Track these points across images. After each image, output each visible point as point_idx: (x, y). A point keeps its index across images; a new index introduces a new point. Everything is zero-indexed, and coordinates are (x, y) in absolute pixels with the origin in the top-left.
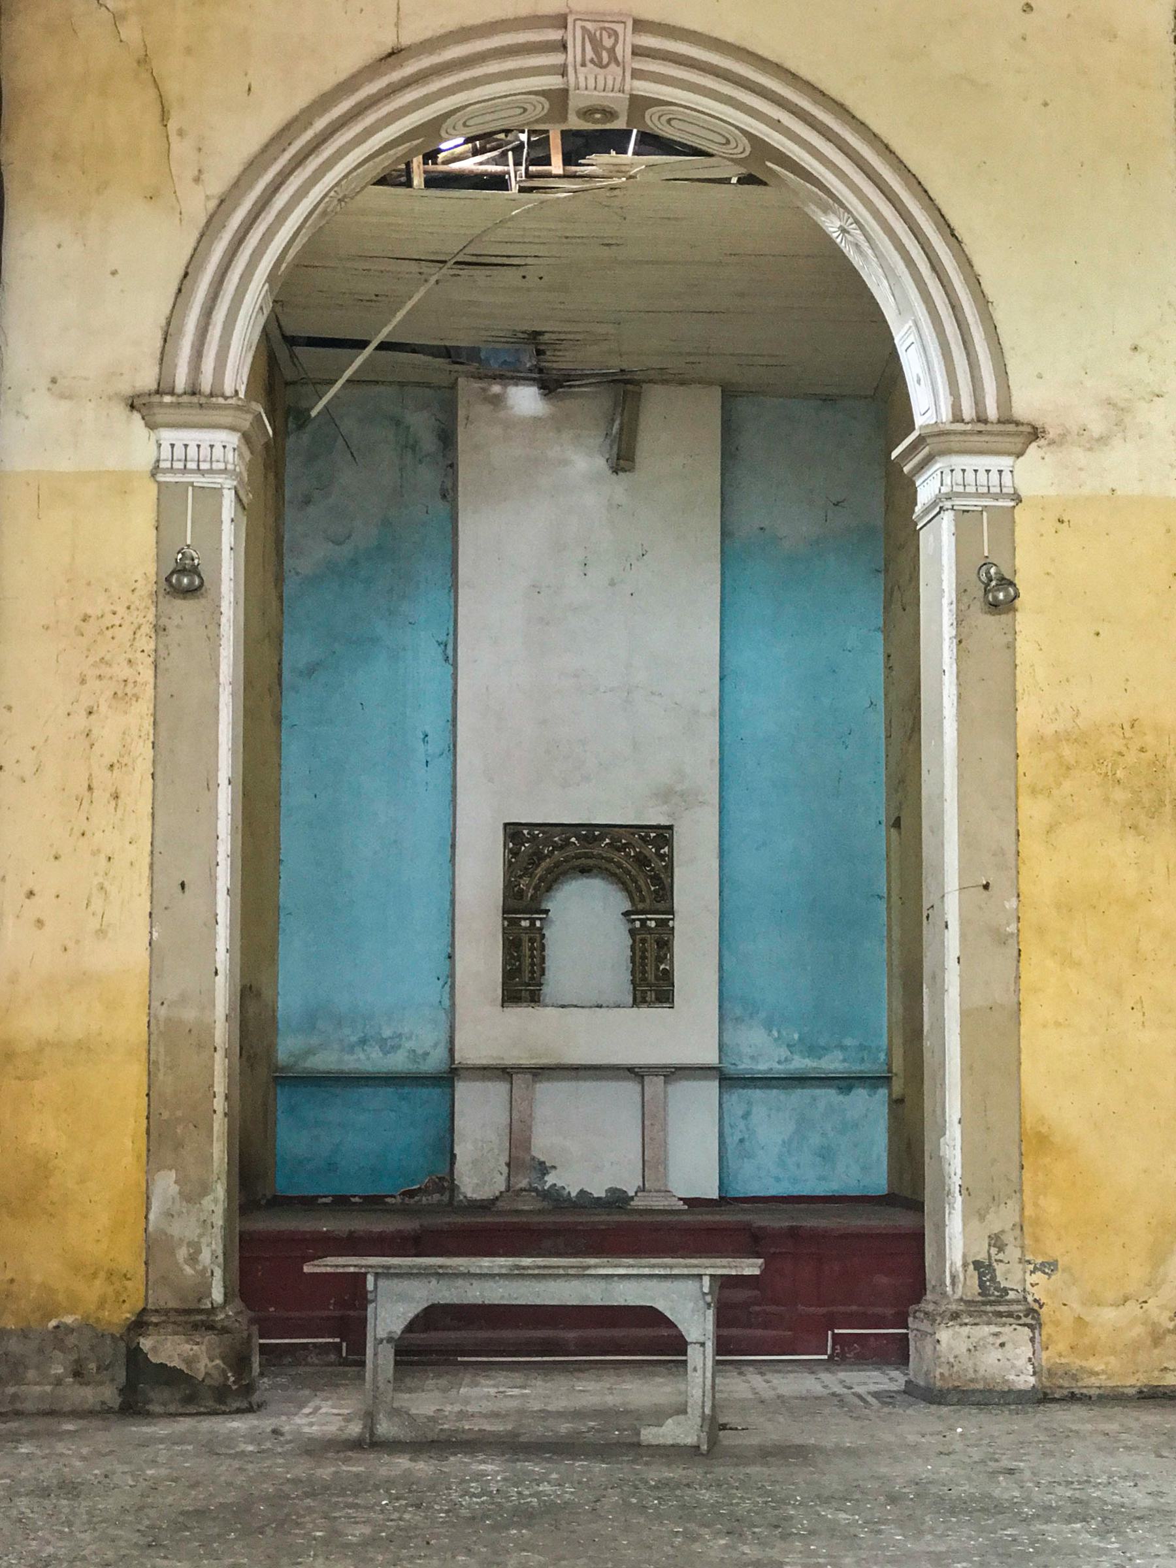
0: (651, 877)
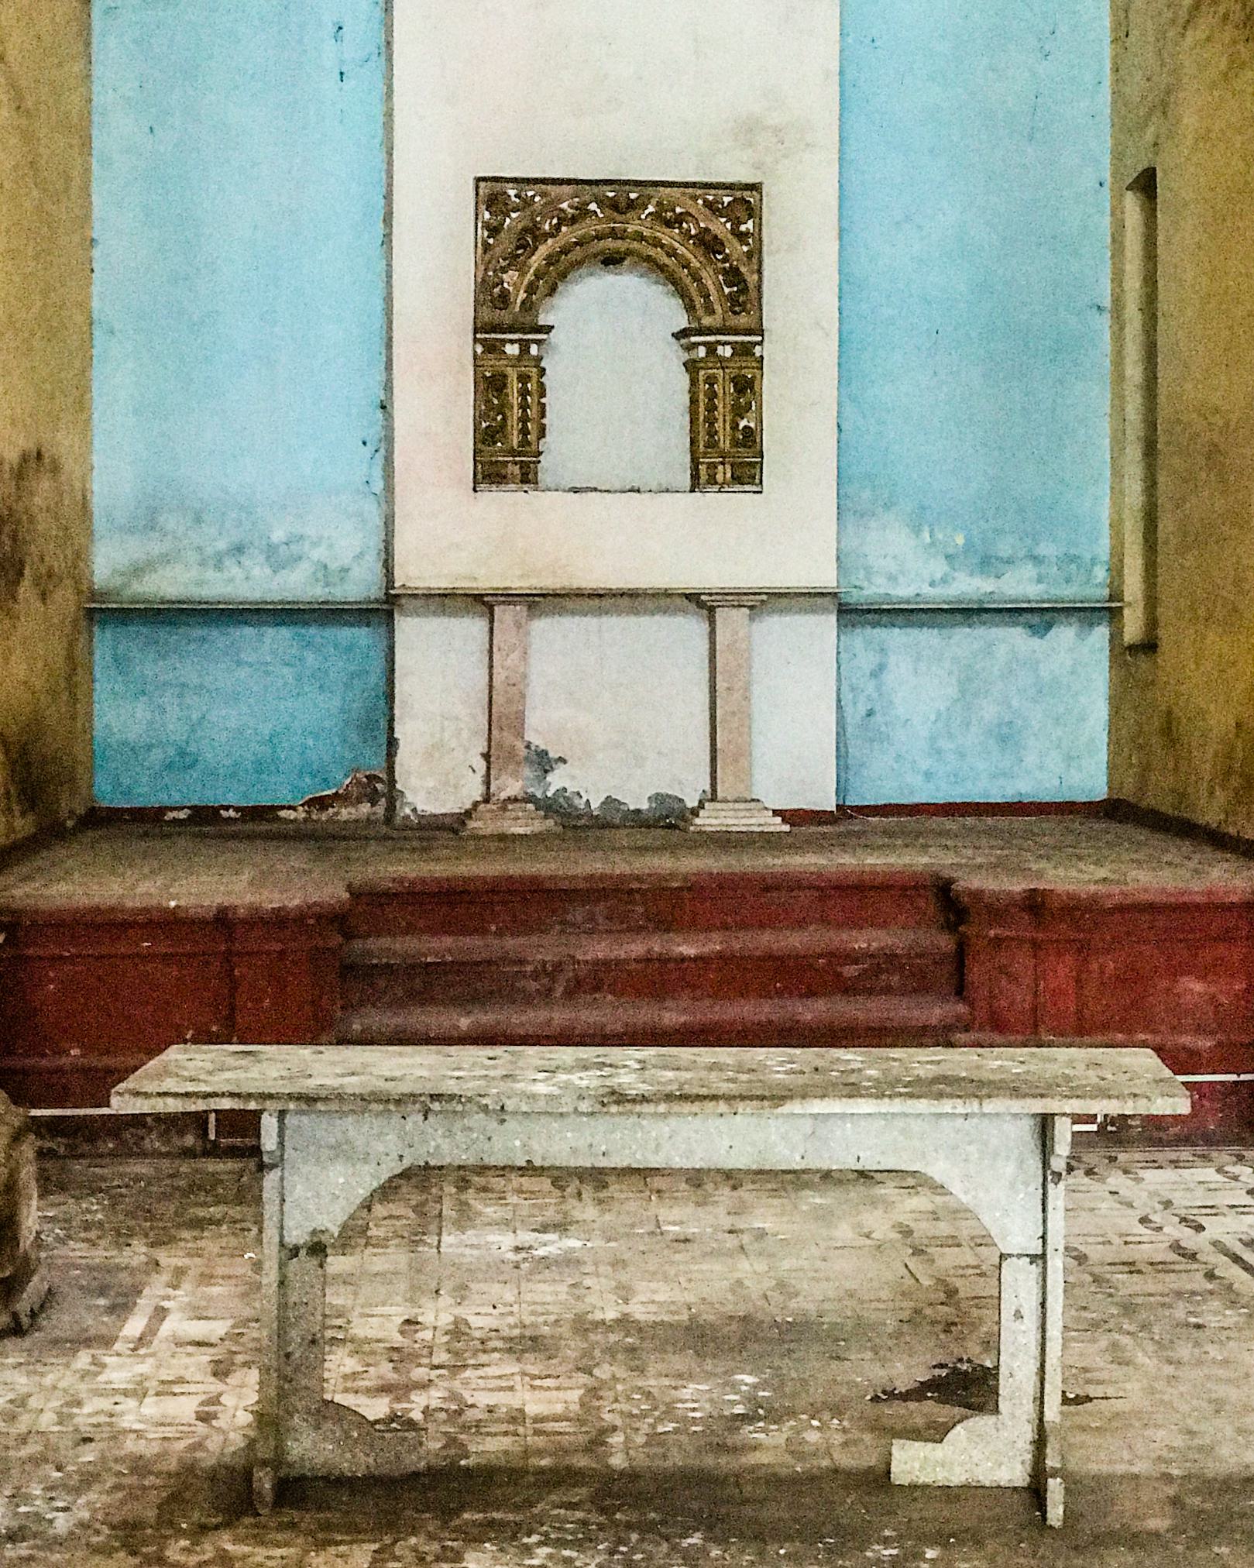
0: (725, 272)
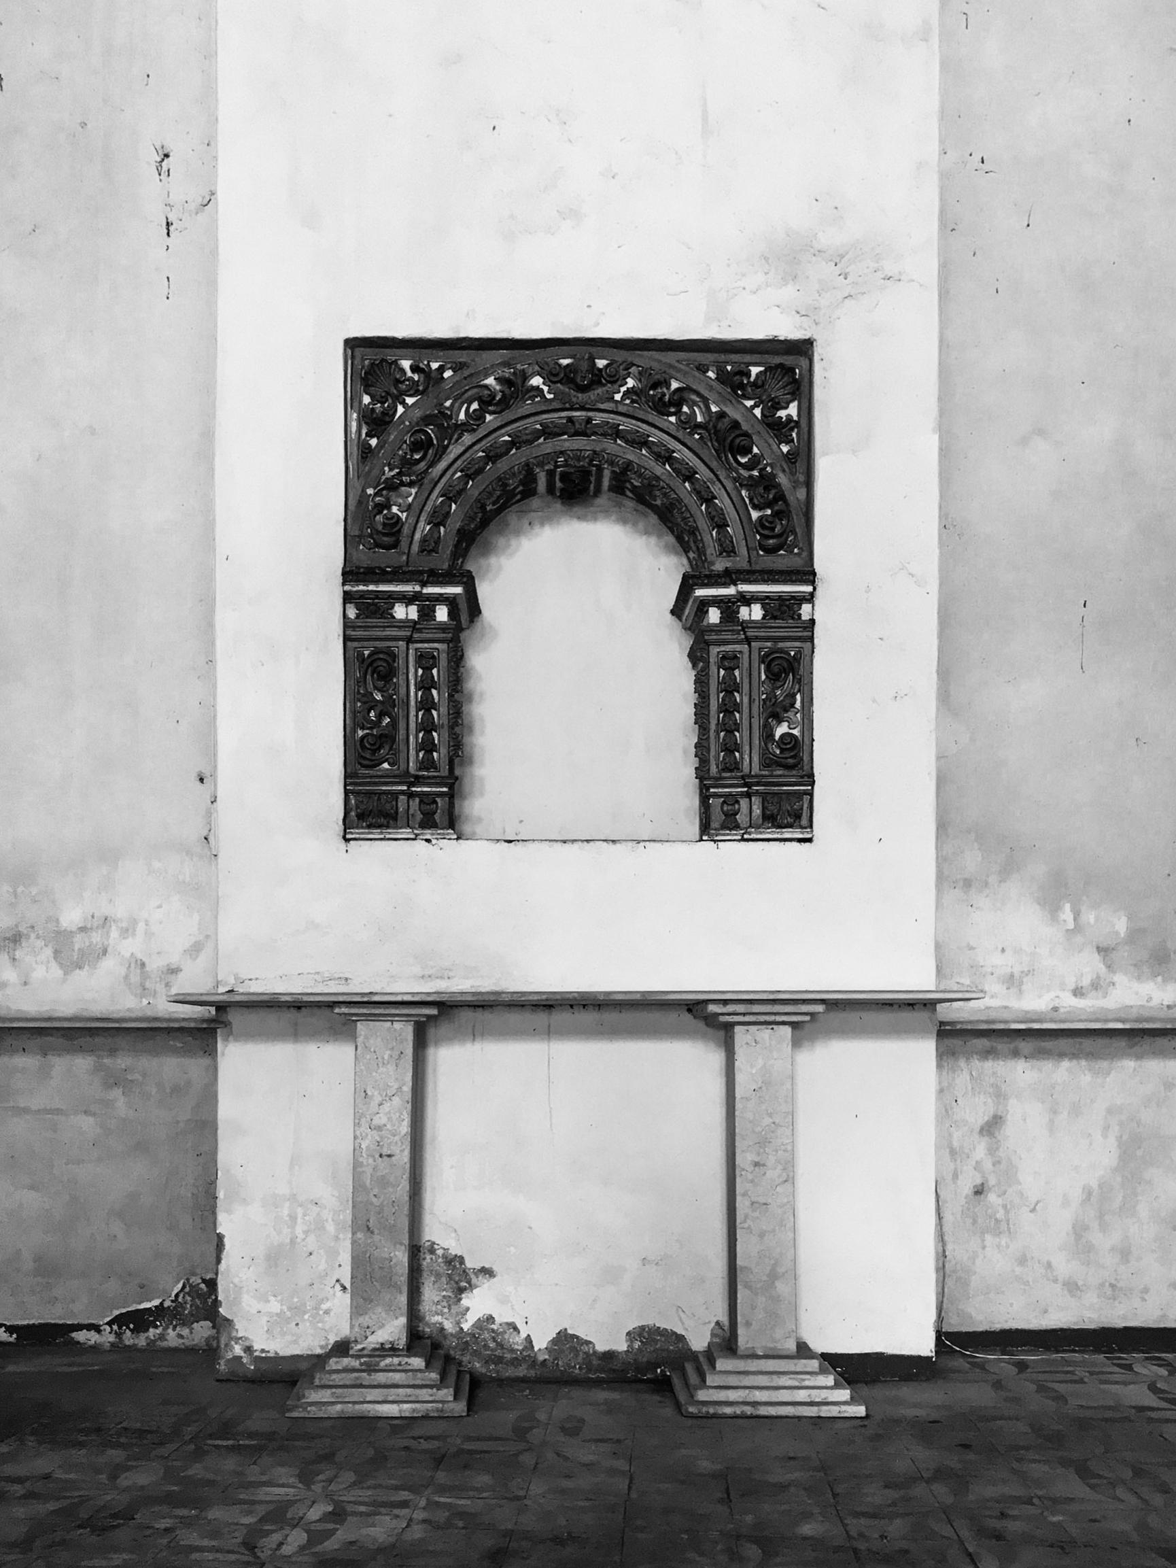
0: (751, 484)
